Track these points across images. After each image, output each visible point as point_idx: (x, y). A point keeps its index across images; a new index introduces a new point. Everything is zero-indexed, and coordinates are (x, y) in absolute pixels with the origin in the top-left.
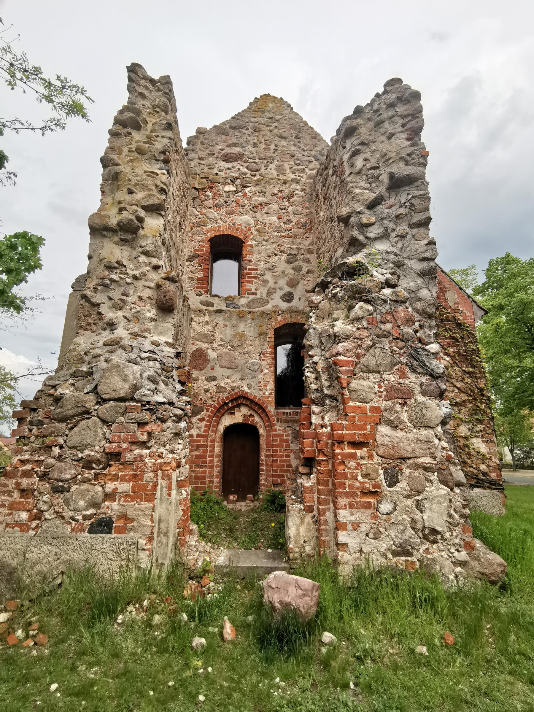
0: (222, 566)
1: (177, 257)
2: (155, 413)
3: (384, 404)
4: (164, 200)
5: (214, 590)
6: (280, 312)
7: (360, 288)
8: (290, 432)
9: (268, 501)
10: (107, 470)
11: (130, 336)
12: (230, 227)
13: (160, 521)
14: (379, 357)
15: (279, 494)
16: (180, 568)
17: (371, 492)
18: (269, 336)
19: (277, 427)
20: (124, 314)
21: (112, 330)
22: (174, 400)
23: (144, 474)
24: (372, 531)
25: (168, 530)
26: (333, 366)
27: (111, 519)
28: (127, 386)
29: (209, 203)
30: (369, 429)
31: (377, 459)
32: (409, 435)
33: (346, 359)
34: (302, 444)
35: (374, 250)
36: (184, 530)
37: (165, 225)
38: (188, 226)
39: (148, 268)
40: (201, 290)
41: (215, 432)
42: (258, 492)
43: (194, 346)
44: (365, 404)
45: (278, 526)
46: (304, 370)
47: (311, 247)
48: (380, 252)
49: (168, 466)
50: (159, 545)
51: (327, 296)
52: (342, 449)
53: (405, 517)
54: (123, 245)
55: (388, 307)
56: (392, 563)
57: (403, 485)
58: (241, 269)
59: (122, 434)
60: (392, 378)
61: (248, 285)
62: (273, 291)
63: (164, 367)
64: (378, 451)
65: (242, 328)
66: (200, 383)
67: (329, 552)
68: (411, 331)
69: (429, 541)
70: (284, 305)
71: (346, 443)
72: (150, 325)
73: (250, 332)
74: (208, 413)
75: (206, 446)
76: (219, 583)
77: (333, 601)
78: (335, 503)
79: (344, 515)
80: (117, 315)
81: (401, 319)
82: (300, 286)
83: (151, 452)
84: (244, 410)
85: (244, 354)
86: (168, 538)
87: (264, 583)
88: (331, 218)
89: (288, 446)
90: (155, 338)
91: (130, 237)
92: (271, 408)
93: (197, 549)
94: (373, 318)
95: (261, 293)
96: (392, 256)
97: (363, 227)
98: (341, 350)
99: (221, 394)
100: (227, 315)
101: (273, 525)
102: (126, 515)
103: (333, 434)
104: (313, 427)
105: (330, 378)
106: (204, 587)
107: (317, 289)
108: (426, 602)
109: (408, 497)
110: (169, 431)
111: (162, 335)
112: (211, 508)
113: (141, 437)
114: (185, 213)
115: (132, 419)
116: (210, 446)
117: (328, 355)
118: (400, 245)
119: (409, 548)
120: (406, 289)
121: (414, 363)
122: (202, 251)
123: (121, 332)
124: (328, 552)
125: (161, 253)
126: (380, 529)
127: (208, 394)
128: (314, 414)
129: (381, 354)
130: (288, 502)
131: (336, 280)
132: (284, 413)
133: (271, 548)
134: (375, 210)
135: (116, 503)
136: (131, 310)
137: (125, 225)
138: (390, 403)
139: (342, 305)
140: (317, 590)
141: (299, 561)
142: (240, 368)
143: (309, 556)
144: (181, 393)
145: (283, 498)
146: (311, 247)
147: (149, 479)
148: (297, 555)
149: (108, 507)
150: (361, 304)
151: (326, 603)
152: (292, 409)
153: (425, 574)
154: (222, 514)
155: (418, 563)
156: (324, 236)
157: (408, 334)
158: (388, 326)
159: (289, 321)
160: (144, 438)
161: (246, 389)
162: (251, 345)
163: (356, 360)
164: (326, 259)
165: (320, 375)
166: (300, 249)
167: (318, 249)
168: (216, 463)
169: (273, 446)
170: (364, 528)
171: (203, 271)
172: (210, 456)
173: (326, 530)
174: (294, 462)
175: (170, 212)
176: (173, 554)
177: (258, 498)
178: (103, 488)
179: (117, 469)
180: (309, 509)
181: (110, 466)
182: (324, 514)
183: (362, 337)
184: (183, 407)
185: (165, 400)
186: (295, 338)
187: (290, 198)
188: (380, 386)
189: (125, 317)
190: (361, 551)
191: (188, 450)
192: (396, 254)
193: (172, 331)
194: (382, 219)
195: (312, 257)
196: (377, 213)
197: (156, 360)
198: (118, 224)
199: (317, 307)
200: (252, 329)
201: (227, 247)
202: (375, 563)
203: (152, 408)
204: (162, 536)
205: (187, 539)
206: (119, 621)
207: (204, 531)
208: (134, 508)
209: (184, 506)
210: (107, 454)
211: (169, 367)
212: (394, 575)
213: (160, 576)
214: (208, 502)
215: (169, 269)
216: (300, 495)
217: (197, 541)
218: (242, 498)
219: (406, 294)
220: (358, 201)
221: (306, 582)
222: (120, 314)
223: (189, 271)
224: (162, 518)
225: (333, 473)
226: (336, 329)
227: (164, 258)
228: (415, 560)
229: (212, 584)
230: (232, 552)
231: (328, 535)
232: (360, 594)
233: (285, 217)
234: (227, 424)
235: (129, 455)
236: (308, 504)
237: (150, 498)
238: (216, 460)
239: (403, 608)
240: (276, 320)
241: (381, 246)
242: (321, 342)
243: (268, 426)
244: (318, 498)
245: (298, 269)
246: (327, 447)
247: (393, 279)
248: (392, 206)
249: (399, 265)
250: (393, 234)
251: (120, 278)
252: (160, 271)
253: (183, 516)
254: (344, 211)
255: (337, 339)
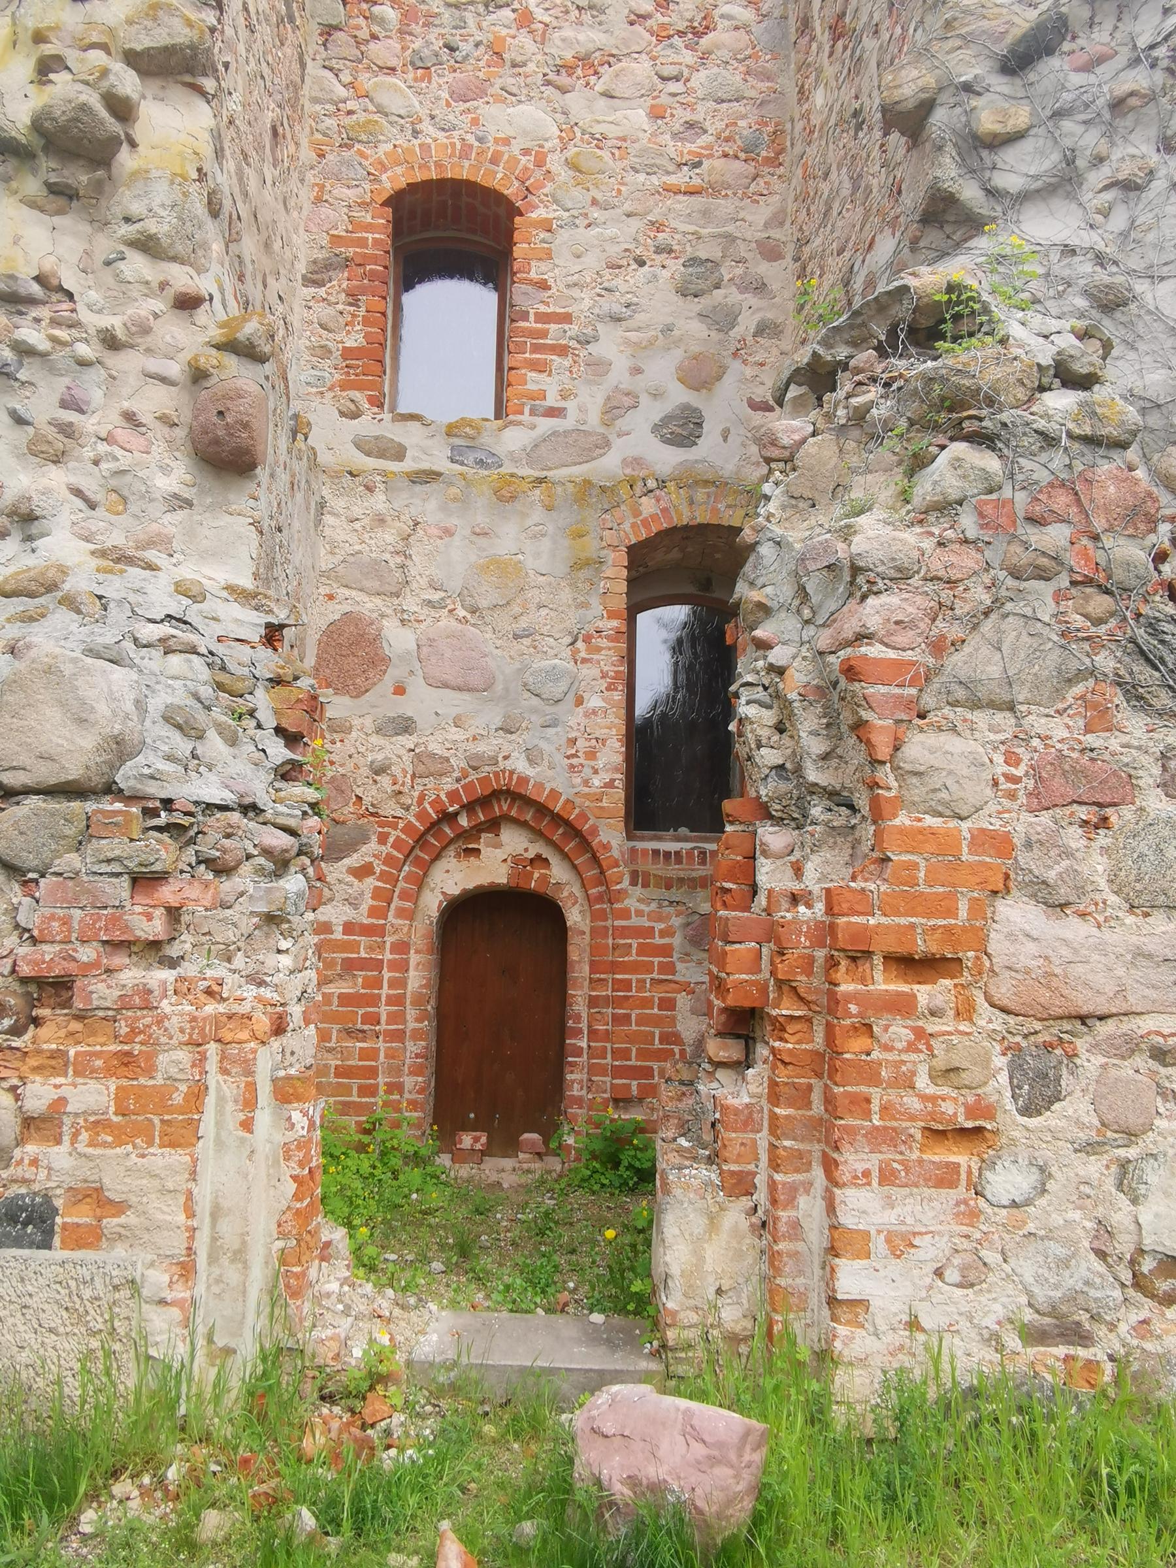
0: (432, 1364)
1: (266, 263)
2: (192, 841)
3: (1023, 824)
4: (212, 30)
5: (405, 1436)
6: (652, 484)
7: (958, 387)
8: (676, 922)
9: (594, 1156)
10: (27, 1037)
11: (95, 562)
12: (466, 148)
13: (215, 1215)
14: (1014, 651)
15: (634, 1133)
16: (287, 1363)
17: (963, 1131)
18: (609, 572)
19: (631, 903)
20: (73, 480)
21: (29, 538)
22: (263, 798)
23: (155, 1054)
24: (956, 1261)
25: (244, 1243)
26: (843, 683)
27: (47, 1199)
28: (88, 741)
29: (385, 51)
30: (963, 913)
31: (987, 1019)
32: (1107, 935)
33: (892, 654)
34: (721, 960)
35: (1014, 240)
36: (298, 1250)
37: (216, 136)
38: (304, 142)
39: (158, 305)
40: (357, 395)
41: (410, 915)
42: (557, 1126)
43: (331, 605)
44: (953, 824)
45: (627, 1239)
46: (737, 695)
47: (776, 234)
48: (1040, 250)
49: (243, 1027)
50: (216, 1289)
51: (829, 417)
52: (863, 981)
53: (1077, 1215)
54: (60, 212)
55: (1058, 460)
56: (1017, 1366)
57: (1075, 1110)
58: (505, 314)
59: (77, 914)
60: (1058, 730)
61: (534, 381)
62: (627, 401)
63: (223, 677)
64: (993, 990)
65: (509, 539)
66: (357, 739)
67: (803, 1328)
68: (1142, 555)
69: (1153, 1297)
70: (666, 459)
71: (878, 960)
72: (172, 523)
73: (537, 555)
74: (386, 849)
75: (378, 965)
76: (423, 1417)
77: (812, 1482)
78: (830, 1166)
79: (862, 1207)
80: (45, 482)
81: (1107, 510)
82: (729, 383)
83: (181, 979)
84: (514, 842)
85: (516, 637)
86: (246, 1266)
87: (578, 1420)
88: (856, 114)
89: (670, 968)
90: (188, 572)
91: (84, 178)
92: (611, 836)
93: (348, 1307)
94: (1000, 504)
95: (582, 409)
96: (1084, 267)
97: (983, 146)
98: (874, 623)
99: (430, 782)
100: (454, 490)
101: (610, 1234)
102: (99, 1190)
103: (832, 927)
104: (762, 900)
105: (828, 726)
106: (372, 1426)
107: (794, 391)
108: (1131, 1493)
109: (1090, 1148)
110: (243, 905)
111: (214, 556)
112: (395, 1175)
113: (145, 924)
114: (297, 88)
115: (109, 861)
116: (393, 966)
117: (824, 640)
118: (1118, 221)
119: (1084, 1317)
120: (1131, 396)
121: (1144, 674)
122: (362, 243)
123: (62, 546)
124: (797, 1327)
125: (205, 246)
126: (983, 1253)
127: (385, 781)
128: (765, 853)
129: (1025, 638)
130: (665, 1161)
131: (866, 356)
132: (656, 852)
133: (602, 1311)
134: (1032, 76)
135: (65, 1146)
136: (96, 463)
137: (64, 130)
138: (1045, 818)
139: (884, 454)
140: (757, 1447)
141: (700, 1353)
142: (499, 687)
143: (734, 1339)
144: (288, 773)
145: (648, 1146)
146: (776, 234)
147: (173, 1071)
148: (691, 1334)
149: (35, 1162)
150: (959, 448)
151: (786, 1488)
152: (686, 839)
153: (1130, 1404)
154: (435, 1197)
155: (1108, 1367)
156: (825, 187)
157: (1128, 565)
158: (1056, 536)
159: (685, 516)
160: (156, 927)
161: (520, 765)
162: (540, 606)
163: (931, 661)
164: (829, 279)
165: (792, 714)
166: (730, 239)
167: (802, 242)
168: (412, 1025)
169: (614, 967)
170: (929, 1250)
171: (366, 322)
172: (390, 1001)
173: (795, 1255)
174: (689, 1026)
175: (234, 80)
176: (264, 1320)
177: (560, 1146)
178: (17, 1098)
179: (62, 1033)
180: (741, 1185)
181: (37, 1022)
182: (791, 1202)
183: (955, 574)
184: (292, 823)
185: (228, 797)
186: (707, 585)
187: (698, 34)
188: (1012, 759)
189: (78, 493)
190: (914, 1324)
191: (312, 974)
192: (1100, 259)
193: (251, 543)
194: (1058, 114)
195: (779, 274)
196: (1040, 89)
197: (193, 651)
198: (37, 125)
199: (790, 459)
200: (546, 544)
201: (453, 231)
202: (961, 1363)
203: (174, 821)
204: (225, 1261)
205: (313, 1273)
206: (86, 1529)
207: (371, 1250)
208: (122, 1168)
209: (301, 1164)
210: (24, 981)
211: (242, 679)
212: (1025, 1402)
213: (220, 1386)
214: (383, 1154)
215: (234, 309)
216: (708, 1137)
217: (344, 1282)
219: (1132, 414)
220: (967, 40)
221: (722, 1421)
222: (57, 478)
223: (313, 324)
224: (225, 1204)
225: (827, 1063)
226: (859, 544)
227: (215, 268)
228: (1102, 1357)
229: (399, 1418)
230: (467, 1318)
231: (801, 1273)
232: (902, 1462)
233: (679, 112)
235: (101, 986)
236: (734, 1167)
237: (181, 1134)
238: (411, 1013)
239: (1049, 1507)
240: (636, 513)
241: (1048, 226)
242: (802, 593)
243: (600, 898)
244: (773, 1147)
245: (723, 320)
246: (809, 973)
247: (1086, 358)
248: (1101, 60)
249: (1110, 302)
250: (1096, 178)
251: (54, 340)
252: (202, 315)
253: (297, 1197)
254: (910, 82)
255: (861, 580)
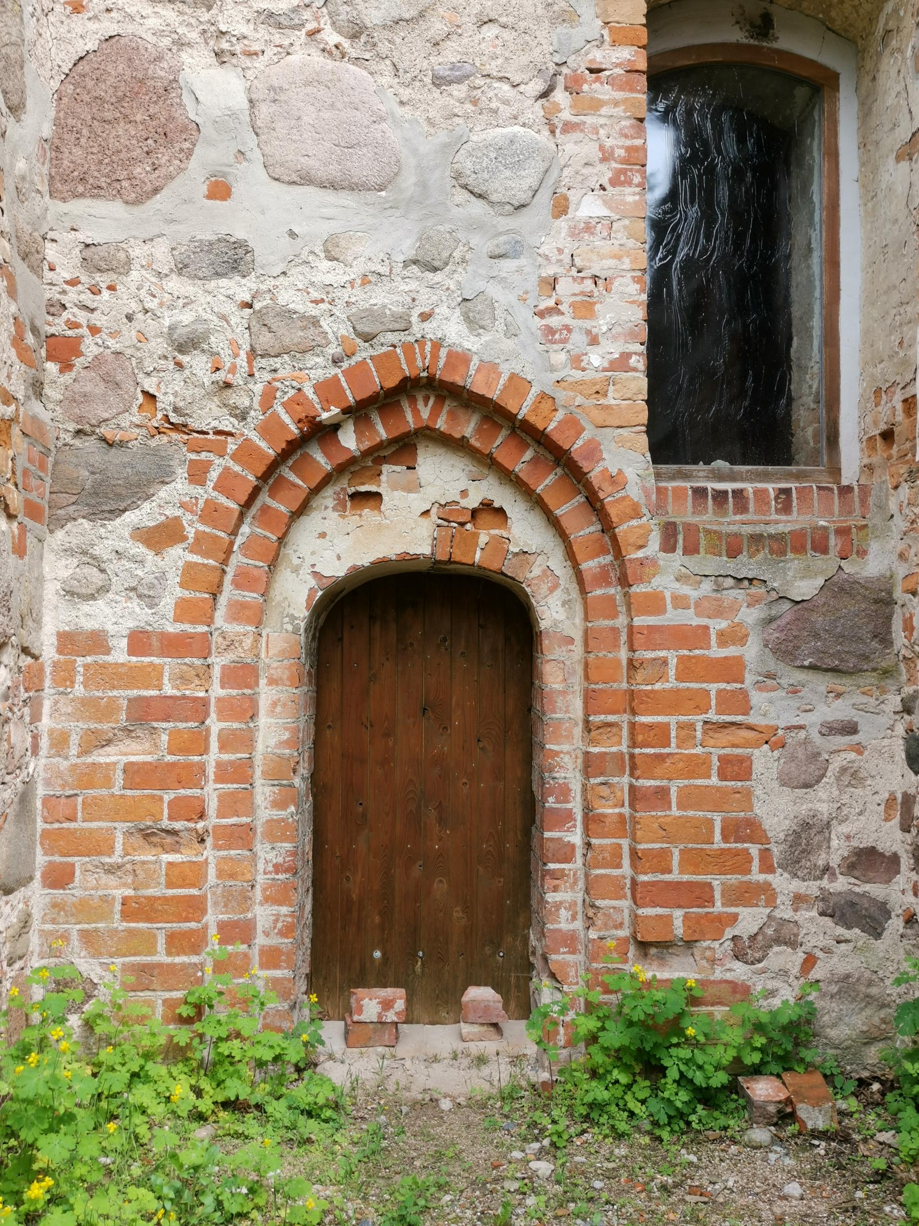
8: (750, 616)
74: (207, 492)
75: (199, 709)
84: (442, 478)
85: (439, 82)
92: (623, 459)
99: (285, 366)
116: (228, 709)
127: (198, 363)
142: (408, 181)
161: (452, 329)
172: (225, 773)
218: (438, 1000)
234: (336, 569)
243: (603, 578)
